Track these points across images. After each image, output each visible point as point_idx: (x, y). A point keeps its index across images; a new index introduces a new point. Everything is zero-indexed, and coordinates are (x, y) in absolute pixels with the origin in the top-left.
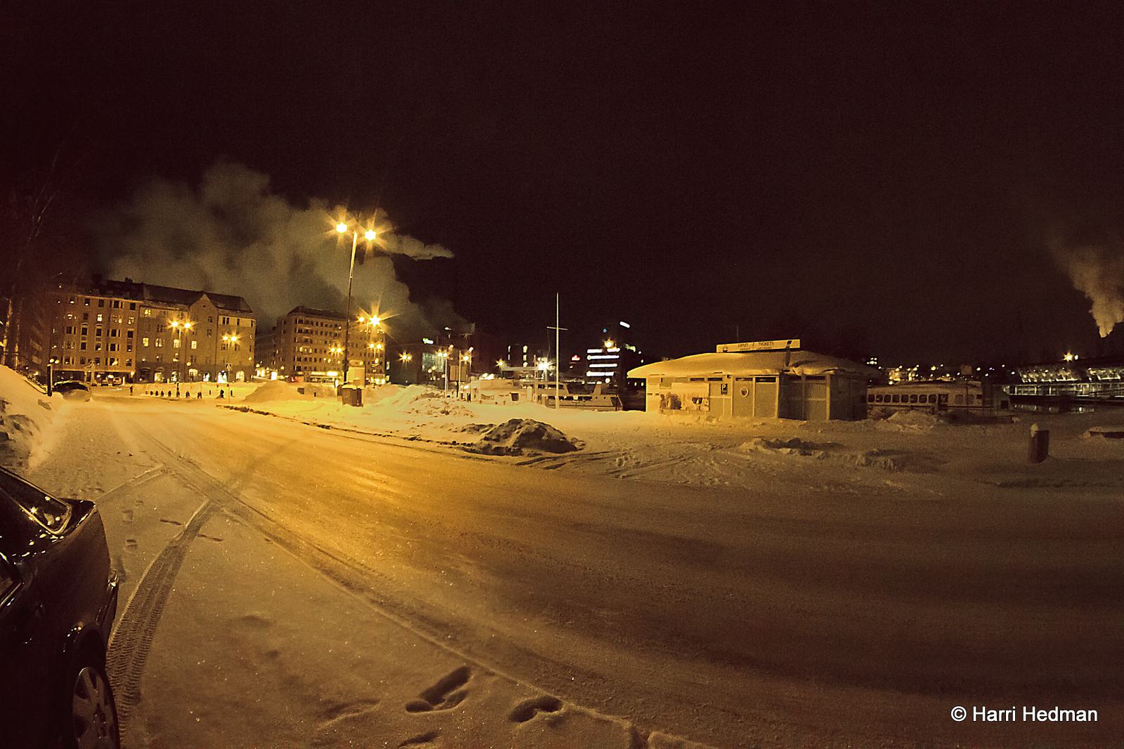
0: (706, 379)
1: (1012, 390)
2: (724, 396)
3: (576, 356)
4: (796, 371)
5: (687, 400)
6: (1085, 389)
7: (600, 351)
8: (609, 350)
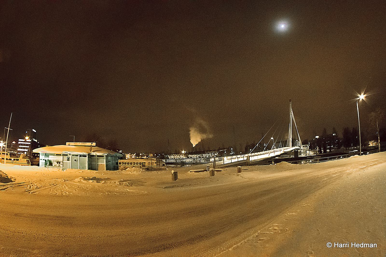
0: (62, 155)
1: (166, 161)
2: (68, 162)
3: (14, 142)
4: (94, 154)
5: (55, 162)
6: (188, 160)
7: (24, 140)
8: (27, 141)
